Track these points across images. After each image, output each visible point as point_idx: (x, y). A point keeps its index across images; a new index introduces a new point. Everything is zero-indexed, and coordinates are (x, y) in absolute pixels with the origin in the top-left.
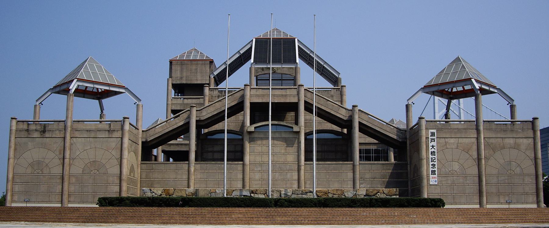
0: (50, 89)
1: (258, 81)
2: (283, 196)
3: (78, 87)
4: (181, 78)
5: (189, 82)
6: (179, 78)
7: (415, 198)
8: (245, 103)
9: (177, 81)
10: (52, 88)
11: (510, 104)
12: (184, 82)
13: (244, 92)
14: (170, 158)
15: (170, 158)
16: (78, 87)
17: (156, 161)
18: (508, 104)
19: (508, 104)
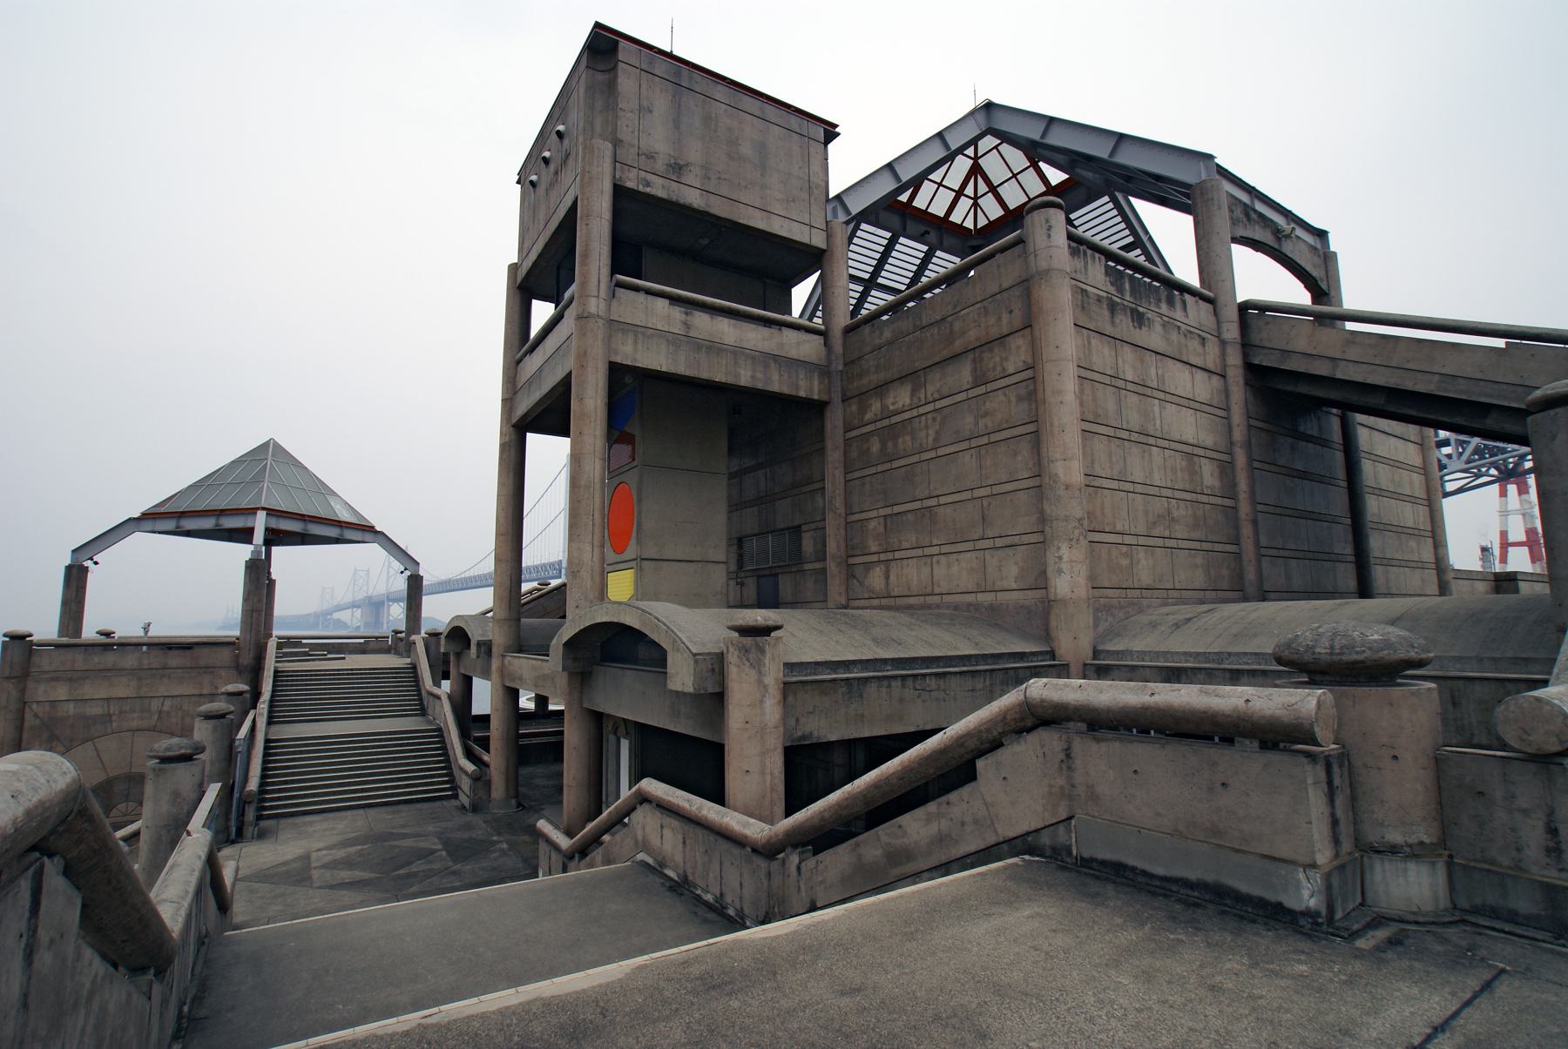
0: (130, 519)
1: (1131, 239)
2: (1313, 415)
3: (1128, 236)
4: (677, 169)
5: (719, 209)
6: (660, 166)
7: (1421, 515)
8: (649, 793)
9: (650, 177)
10: (137, 515)
11: (408, 573)
12: (694, 198)
13: (1025, 247)
14: (1067, 176)
15: (1067, 176)
16: (1128, 236)
17: (1445, 595)
18: (402, 572)
19: (402, 572)
